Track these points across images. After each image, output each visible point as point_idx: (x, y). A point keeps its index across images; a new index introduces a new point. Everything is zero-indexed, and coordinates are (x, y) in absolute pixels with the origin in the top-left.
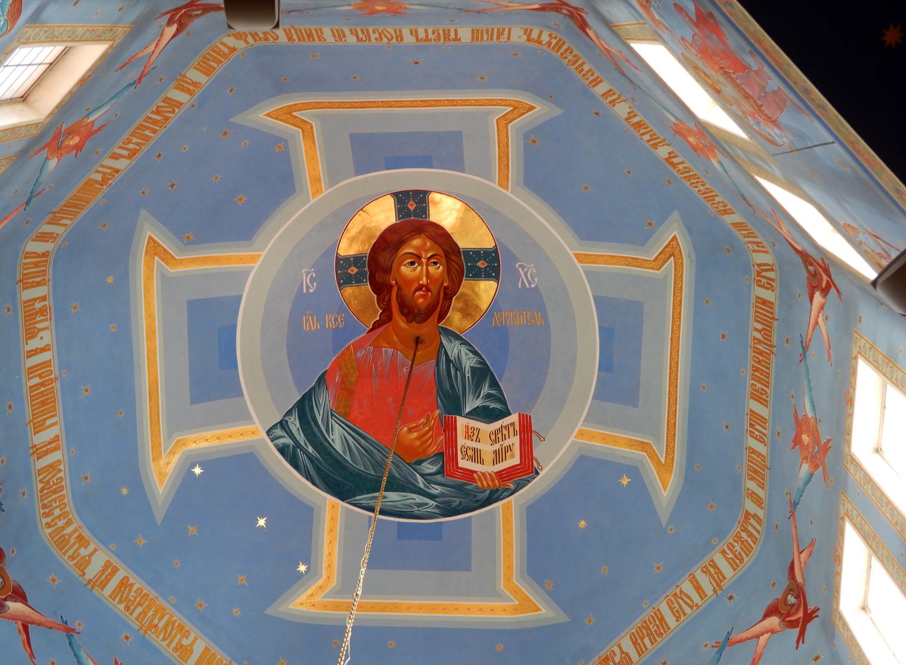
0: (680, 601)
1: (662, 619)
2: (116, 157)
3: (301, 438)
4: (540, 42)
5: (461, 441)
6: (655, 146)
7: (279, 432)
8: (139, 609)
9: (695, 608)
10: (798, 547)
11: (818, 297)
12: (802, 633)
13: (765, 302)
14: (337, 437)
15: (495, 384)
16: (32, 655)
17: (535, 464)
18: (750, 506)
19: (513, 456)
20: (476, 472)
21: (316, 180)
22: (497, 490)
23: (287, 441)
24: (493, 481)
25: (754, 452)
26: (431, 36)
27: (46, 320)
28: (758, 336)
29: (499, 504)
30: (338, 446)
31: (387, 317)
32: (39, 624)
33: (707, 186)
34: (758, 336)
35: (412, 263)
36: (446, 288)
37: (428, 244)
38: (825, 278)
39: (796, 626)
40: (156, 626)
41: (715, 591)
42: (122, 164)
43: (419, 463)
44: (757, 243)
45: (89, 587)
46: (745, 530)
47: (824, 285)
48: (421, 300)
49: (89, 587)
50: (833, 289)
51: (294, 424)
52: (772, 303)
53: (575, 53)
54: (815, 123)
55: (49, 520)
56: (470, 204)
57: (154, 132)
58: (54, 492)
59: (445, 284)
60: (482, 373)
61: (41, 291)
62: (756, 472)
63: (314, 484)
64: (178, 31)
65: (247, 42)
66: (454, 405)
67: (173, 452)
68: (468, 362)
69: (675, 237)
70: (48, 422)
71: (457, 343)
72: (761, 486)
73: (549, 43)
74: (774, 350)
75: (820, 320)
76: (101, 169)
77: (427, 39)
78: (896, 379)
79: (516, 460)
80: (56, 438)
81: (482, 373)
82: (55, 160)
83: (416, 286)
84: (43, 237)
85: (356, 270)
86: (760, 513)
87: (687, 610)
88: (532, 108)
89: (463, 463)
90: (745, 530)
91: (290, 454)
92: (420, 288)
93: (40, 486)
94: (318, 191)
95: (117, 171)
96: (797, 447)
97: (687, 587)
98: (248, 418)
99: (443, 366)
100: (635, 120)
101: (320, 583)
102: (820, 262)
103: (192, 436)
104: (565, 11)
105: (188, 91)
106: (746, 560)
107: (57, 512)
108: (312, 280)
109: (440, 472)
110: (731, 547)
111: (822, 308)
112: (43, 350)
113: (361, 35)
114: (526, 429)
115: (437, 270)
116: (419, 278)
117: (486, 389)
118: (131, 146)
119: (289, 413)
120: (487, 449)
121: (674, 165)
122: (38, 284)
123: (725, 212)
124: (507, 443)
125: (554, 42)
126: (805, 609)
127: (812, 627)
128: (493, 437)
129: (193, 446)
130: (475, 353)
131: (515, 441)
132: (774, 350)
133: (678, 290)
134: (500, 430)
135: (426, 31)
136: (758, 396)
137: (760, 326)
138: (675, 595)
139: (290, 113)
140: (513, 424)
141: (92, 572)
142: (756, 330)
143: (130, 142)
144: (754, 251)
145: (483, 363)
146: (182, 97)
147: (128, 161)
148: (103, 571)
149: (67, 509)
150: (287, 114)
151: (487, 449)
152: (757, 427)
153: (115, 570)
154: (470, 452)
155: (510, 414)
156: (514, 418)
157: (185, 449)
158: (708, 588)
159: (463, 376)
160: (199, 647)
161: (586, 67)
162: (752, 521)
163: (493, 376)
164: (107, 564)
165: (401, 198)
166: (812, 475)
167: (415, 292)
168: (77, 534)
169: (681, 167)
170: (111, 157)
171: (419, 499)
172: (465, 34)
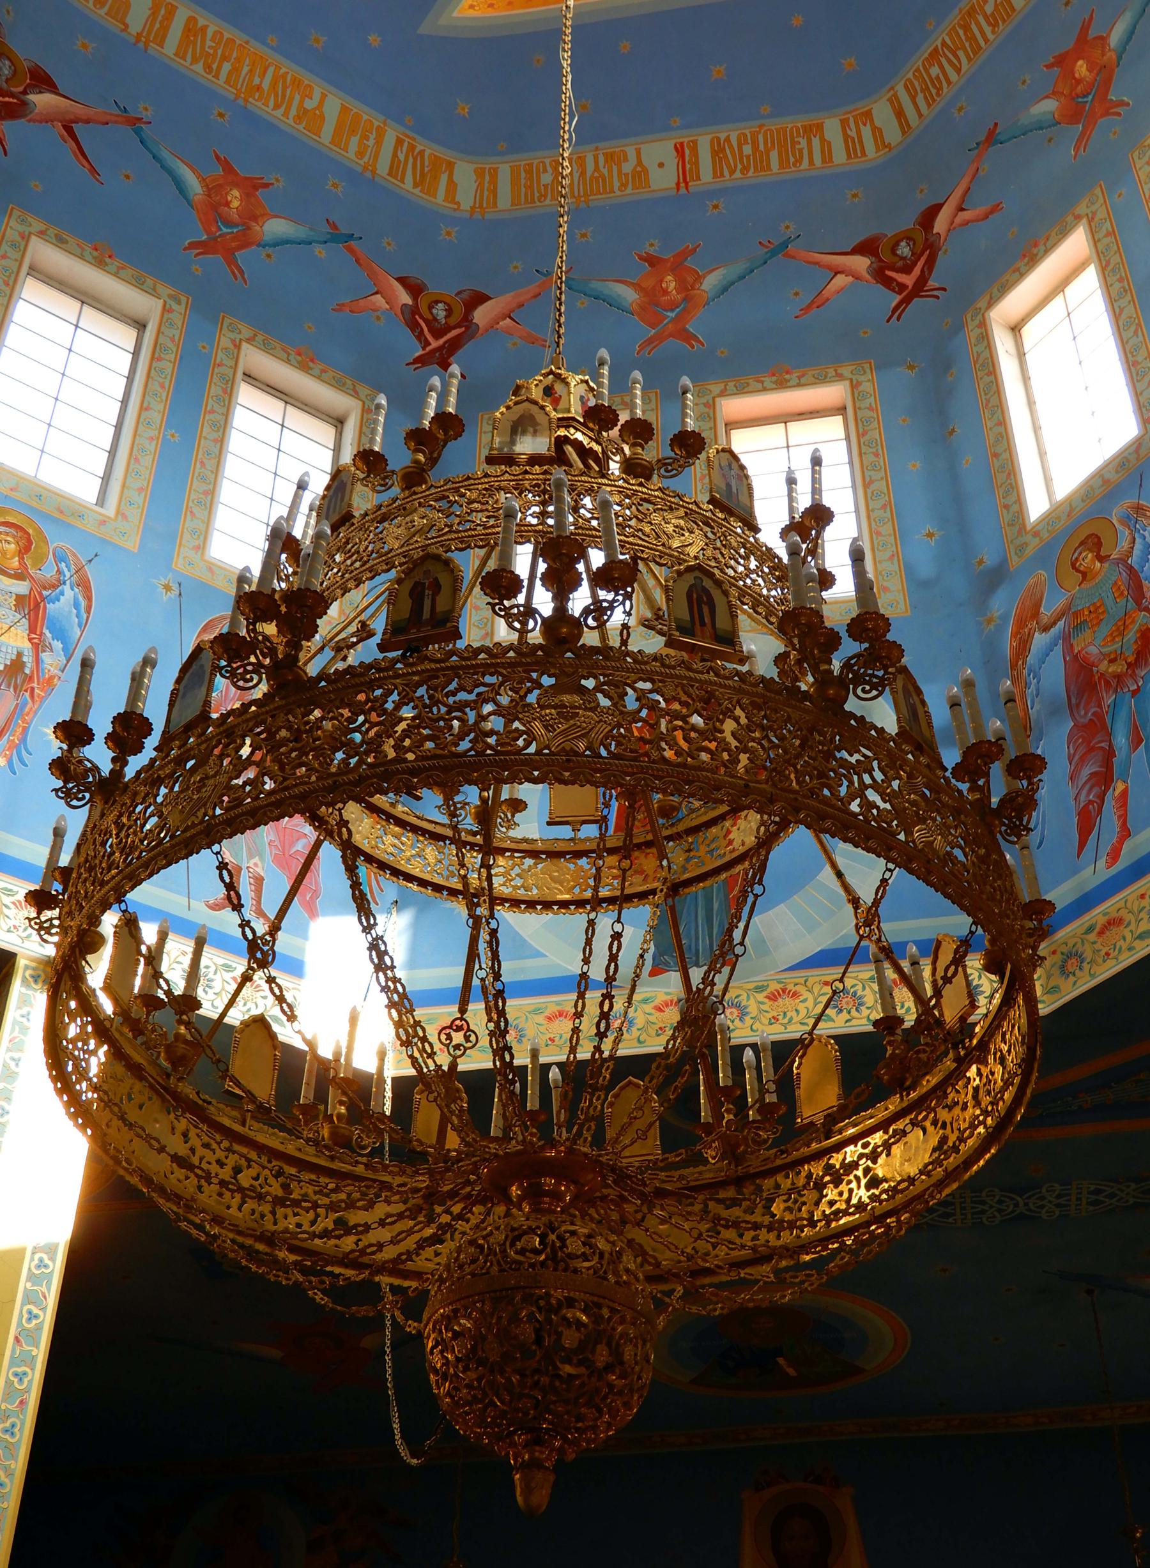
8: (227, 67)
11: (861, 263)
16: (93, 171)
32: (88, 121)
45: (141, 45)
49: (141, 45)
160: (333, 106)
162: (816, 142)
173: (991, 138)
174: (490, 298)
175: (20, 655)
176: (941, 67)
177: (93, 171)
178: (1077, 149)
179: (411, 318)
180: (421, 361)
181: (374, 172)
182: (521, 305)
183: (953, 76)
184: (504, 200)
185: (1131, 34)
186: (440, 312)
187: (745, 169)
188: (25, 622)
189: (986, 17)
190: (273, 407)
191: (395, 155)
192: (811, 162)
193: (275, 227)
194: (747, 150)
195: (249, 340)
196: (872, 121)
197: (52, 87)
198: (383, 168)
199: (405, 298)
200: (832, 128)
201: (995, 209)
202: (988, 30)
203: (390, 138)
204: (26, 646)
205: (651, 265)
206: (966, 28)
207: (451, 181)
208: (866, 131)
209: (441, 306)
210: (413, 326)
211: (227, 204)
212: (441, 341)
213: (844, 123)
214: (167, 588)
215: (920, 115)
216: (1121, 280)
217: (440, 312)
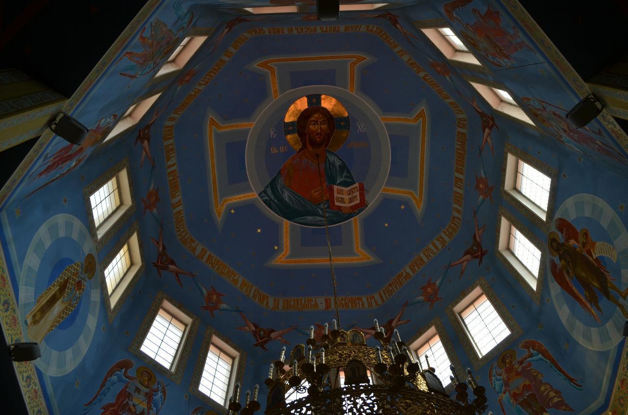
0: (429, 252)
1: (421, 259)
2: (200, 85)
3: (272, 197)
4: (372, 31)
5: (336, 195)
6: (418, 72)
7: (263, 194)
8: (217, 266)
9: (435, 254)
10: (478, 228)
11: (487, 130)
12: (481, 260)
13: (462, 134)
14: (286, 195)
15: (348, 172)
16: (181, 285)
17: (366, 203)
18: (455, 214)
19: (357, 200)
20: (342, 207)
21: (276, 92)
22: (351, 214)
23: (267, 198)
24: (349, 210)
25: (457, 193)
26: (328, 30)
27: (173, 153)
28: (459, 147)
29: (352, 219)
30: (287, 199)
31: (304, 146)
32: (181, 273)
33: (435, 89)
34: (459, 147)
35: (314, 124)
36: (328, 134)
37: (321, 116)
38: (491, 122)
39: (478, 258)
40: (224, 272)
41: (442, 247)
42: (202, 88)
43: (320, 204)
44: (459, 110)
45: (197, 258)
46: (453, 223)
47: (490, 125)
48: (318, 139)
49: (197, 258)
50: (495, 127)
51: (269, 192)
52: (466, 134)
53: (387, 35)
54: (537, 55)
55: (179, 233)
56: (339, 99)
57: (215, 73)
58: (181, 222)
59: (328, 132)
60: (343, 168)
61: (171, 141)
62: (458, 201)
63: (278, 214)
64: (229, 30)
65: (252, 35)
66: (333, 181)
67: (223, 205)
68: (338, 163)
69: (423, 109)
70: (176, 195)
71: (333, 156)
72: (460, 206)
73: (376, 31)
74: (466, 152)
75: (488, 139)
76: (194, 90)
77: (326, 31)
78: (528, 160)
79: (358, 201)
80: (180, 201)
81: (343, 168)
82: (180, 87)
83: (316, 133)
84: (172, 119)
85: (342, 123)
86: (460, 216)
87: (431, 255)
88: (365, 58)
89: (337, 204)
90: (453, 223)
91: (268, 203)
92: (318, 134)
93: (175, 220)
94: (276, 96)
95: (200, 90)
96: (477, 190)
97: (431, 246)
98: (251, 190)
99: (328, 164)
100: (411, 62)
101: (283, 253)
102: (490, 116)
103: (230, 198)
104: (388, 18)
105: (229, 56)
106: (454, 234)
107: (182, 230)
108: (274, 133)
109: (328, 207)
110: (447, 230)
111: (489, 134)
112: (173, 165)
113: (299, 30)
114: (362, 189)
115: (324, 127)
116: (317, 130)
117: (345, 174)
118: (206, 80)
119: (267, 187)
120: (346, 197)
121: (426, 80)
122: (170, 138)
123: (447, 98)
124: (354, 194)
125: (378, 31)
126: (481, 251)
127: (485, 258)
128: (349, 193)
129: (231, 202)
130: (340, 159)
131: (357, 194)
132: (466, 152)
133: (424, 130)
134: (350, 190)
135: (327, 28)
136: (459, 171)
137: (460, 143)
138: (426, 250)
139: (358, 59)
140: (356, 187)
141: (197, 252)
142: (458, 145)
143: (206, 78)
144: (457, 113)
145: (343, 163)
146: (226, 59)
147: (204, 86)
148: (202, 252)
149: (185, 228)
150: (265, 65)
151: (346, 197)
152: (458, 183)
153: (206, 252)
154: (339, 199)
155: (355, 183)
156: (357, 185)
157: (227, 203)
158: (440, 247)
159: (336, 169)
160: (241, 280)
161: (391, 41)
162: (456, 220)
163: (348, 168)
164: (203, 249)
165: (310, 98)
166: (484, 200)
167: (315, 136)
168: (190, 239)
169: (429, 80)
170: (199, 85)
171: (320, 219)
172: (342, 29)
173: (406, 304)
174: (275, 331)
175: (144, 410)
176: (392, 287)
177: (181, 285)
178: (430, 308)
179: (255, 333)
180: (256, 345)
181: (249, 296)
182: (284, 334)
183: (395, 290)
184: (281, 307)
185: (441, 283)
186: (262, 333)
187: (343, 306)
188: (146, 400)
189: (403, 277)
190: (217, 351)
191: (254, 293)
192: (359, 306)
193: (224, 306)
194: (343, 302)
195: (214, 333)
196: (374, 298)
197: (175, 265)
198: (251, 295)
199: (253, 328)
200: (364, 299)
201: (409, 321)
202: (404, 280)
203: (254, 288)
204: (146, 407)
205: (319, 327)
206: (398, 279)
207: (267, 301)
208: (373, 301)
209: (262, 332)
210: (255, 336)
211: (213, 298)
212: (262, 340)
213: (367, 299)
214: (186, 397)
215: (387, 298)
216: (446, 339)
217: (262, 333)
